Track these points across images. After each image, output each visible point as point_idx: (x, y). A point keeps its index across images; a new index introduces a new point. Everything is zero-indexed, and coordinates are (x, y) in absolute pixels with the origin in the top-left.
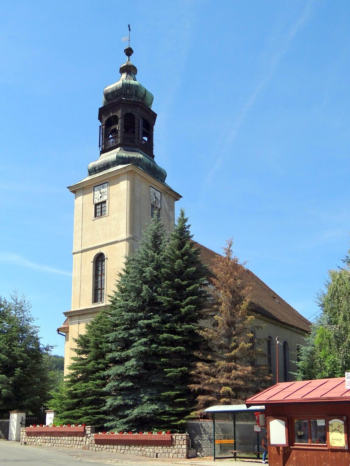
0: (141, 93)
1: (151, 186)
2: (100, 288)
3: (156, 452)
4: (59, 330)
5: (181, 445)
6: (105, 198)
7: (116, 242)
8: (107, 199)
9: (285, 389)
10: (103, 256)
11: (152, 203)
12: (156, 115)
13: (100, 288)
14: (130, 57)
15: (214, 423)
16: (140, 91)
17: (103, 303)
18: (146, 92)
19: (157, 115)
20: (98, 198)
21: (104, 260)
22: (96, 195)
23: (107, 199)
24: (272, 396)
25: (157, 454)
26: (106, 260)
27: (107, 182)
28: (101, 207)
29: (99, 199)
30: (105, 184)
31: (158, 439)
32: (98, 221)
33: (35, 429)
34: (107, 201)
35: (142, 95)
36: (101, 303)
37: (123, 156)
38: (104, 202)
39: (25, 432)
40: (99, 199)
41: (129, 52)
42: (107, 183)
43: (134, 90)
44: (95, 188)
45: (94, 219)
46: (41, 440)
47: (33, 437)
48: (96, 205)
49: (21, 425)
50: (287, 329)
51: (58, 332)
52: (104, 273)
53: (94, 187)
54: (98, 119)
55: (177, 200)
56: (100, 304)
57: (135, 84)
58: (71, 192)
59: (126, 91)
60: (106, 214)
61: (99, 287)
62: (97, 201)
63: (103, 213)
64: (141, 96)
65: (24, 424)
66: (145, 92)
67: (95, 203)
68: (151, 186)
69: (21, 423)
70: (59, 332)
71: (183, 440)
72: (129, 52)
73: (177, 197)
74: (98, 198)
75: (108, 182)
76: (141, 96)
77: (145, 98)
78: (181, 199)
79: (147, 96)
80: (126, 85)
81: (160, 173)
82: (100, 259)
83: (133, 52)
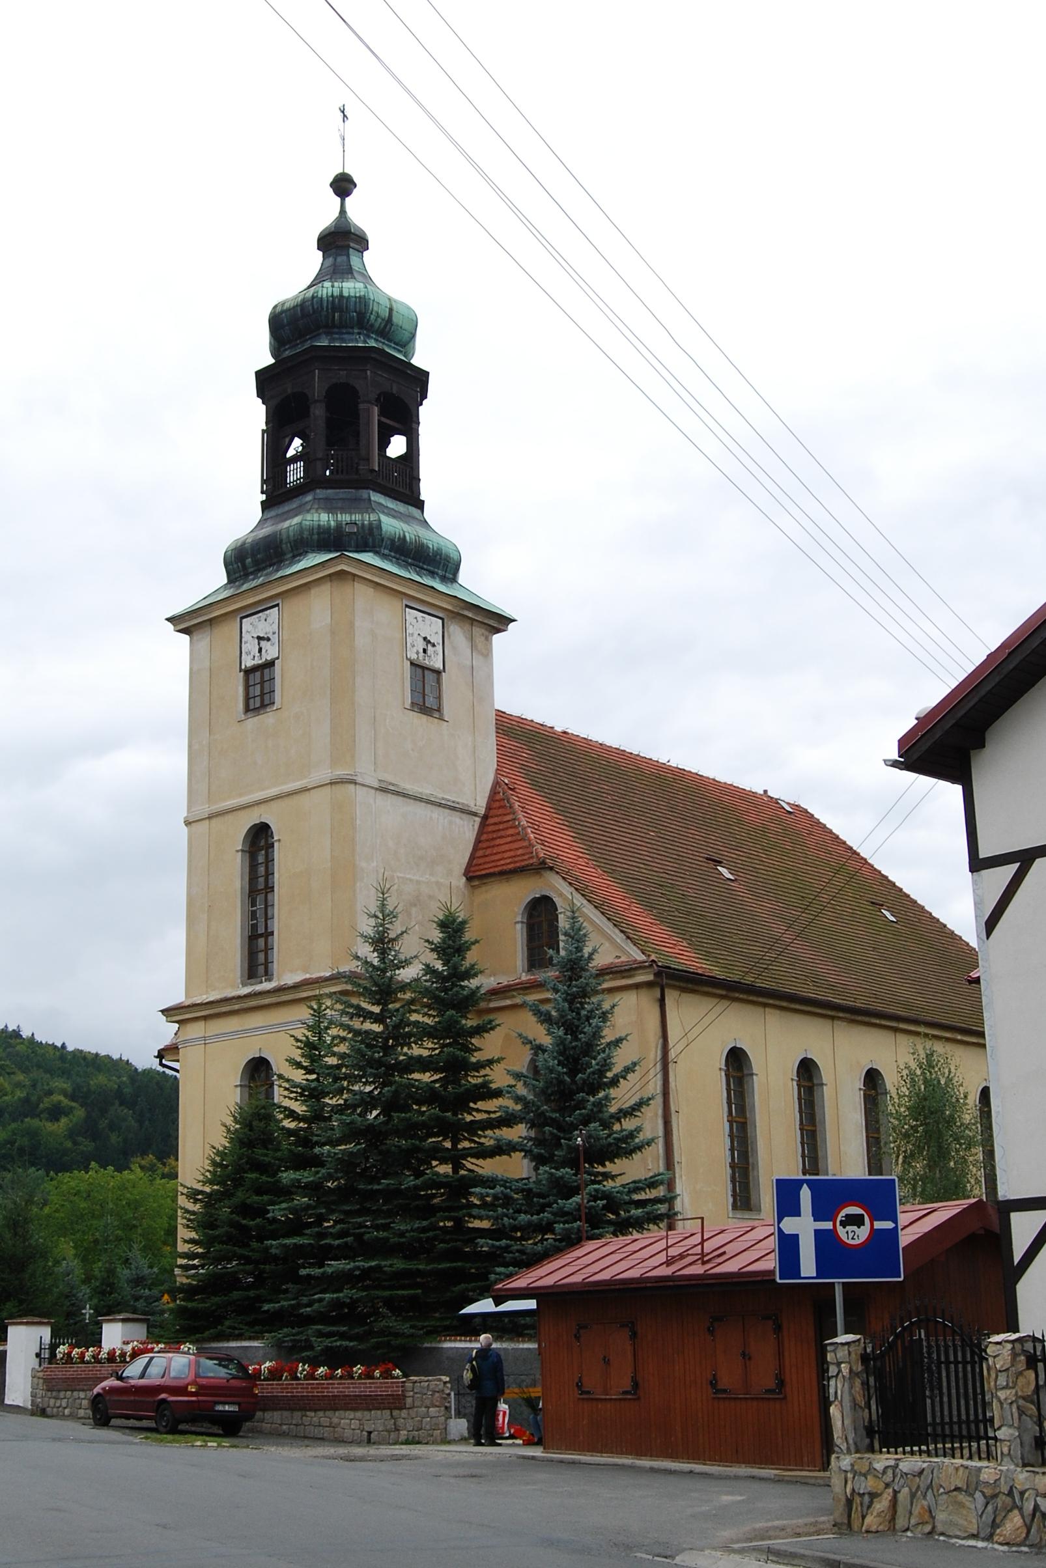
0: (378, 316)
1: (407, 606)
2: (263, 931)
3: (367, 1429)
4: (163, 1053)
5: (425, 1407)
6: (271, 652)
7: (306, 790)
8: (278, 658)
9: (761, 1241)
10: (270, 834)
11: (414, 656)
12: (426, 374)
13: (263, 931)
14: (348, 200)
15: (780, 1354)
16: (372, 313)
17: (270, 980)
18: (391, 310)
19: (426, 374)
20: (252, 654)
21: (272, 846)
22: (246, 643)
23: (278, 658)
24: (566, 1267)
25: (370, 1433)
26: (276, 845)
27: (277, 605)
28: (262, 682)
29: (254, 657)
30: (272, 610)
31: (370, 1392)
32: (253, 722)
33: (66, 1371)
34: (276, 661)
35: (379, 320)
36: (266, 981)
37: (322, 523)
38: (270, 664)
39: (41, 1381)
40: (254, 657)
41: (343, 186)
42: (277, 608)
43: (356, 312)
44: (244, 620)
45: (243, 717)
46: (83, 1401)
47: (62, 1394)
48: (248, 672)
49: (38, 1360)
50: (896, 1030)
51: (161, 1061)
52: (273, 887)
53: (242, 618)
54: (258, 396)
55: (498, 631)
56: (261, 982)
57: (358, 295)
58: (179, 631)
59: (331, 317)
60: (274, 703)
61: (261, 930)
62: (248, 662)
63: (267, 697)
64: (377, 325)
65: (45, 1358)
66: (388, 310)
67: (243, 667)
68: (407, 606)
69: (38, 1355)
70: (164, 1062)
71: (430, 1393)
72: (343, 186)
73: (498, 622)
74: (252, 654)
75: (280, 605)
76: (377, 325)
77: (390, 328)
78: (511, 625)
79: (395, 320)
80: (331, 299)
81: (438, 557)
82: (263, 843)
83: (355, 186)
